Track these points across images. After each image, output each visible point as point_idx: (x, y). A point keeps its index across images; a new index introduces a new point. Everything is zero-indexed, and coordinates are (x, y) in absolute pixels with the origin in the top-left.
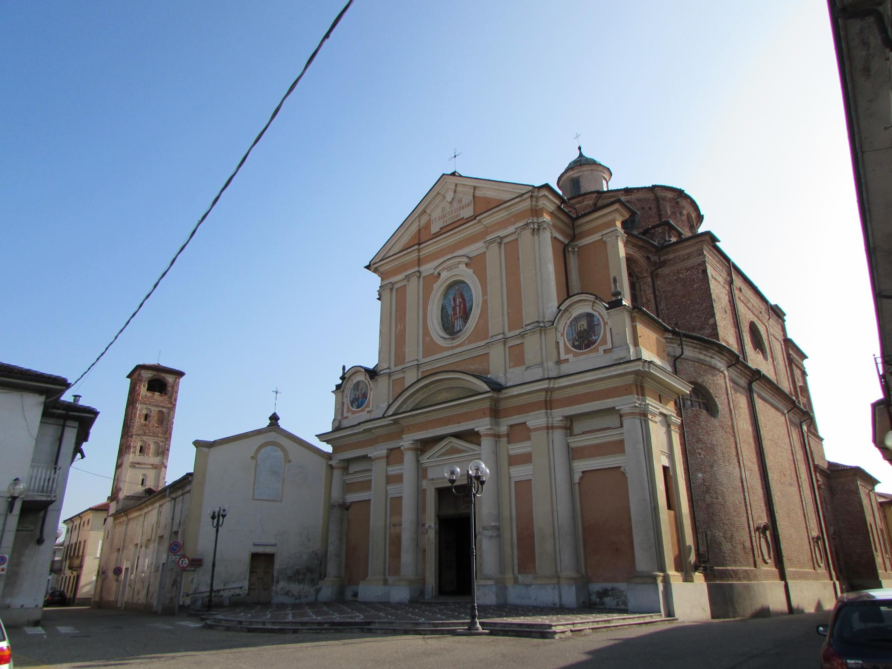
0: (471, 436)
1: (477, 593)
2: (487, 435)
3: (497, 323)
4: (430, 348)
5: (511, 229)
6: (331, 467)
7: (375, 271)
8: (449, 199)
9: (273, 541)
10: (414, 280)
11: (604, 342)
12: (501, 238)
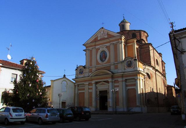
0: (108, 82)
1: (108, 109)
2: (110, 82)
3: (112, 60)
4: (97, 63)
5: (116, 42)
6: (75, 86)
7: (85, 46)
8: (102, 33)
9: (65, 100)
10: (94, 49)
11: (133, 66)
12: (114, 43)
